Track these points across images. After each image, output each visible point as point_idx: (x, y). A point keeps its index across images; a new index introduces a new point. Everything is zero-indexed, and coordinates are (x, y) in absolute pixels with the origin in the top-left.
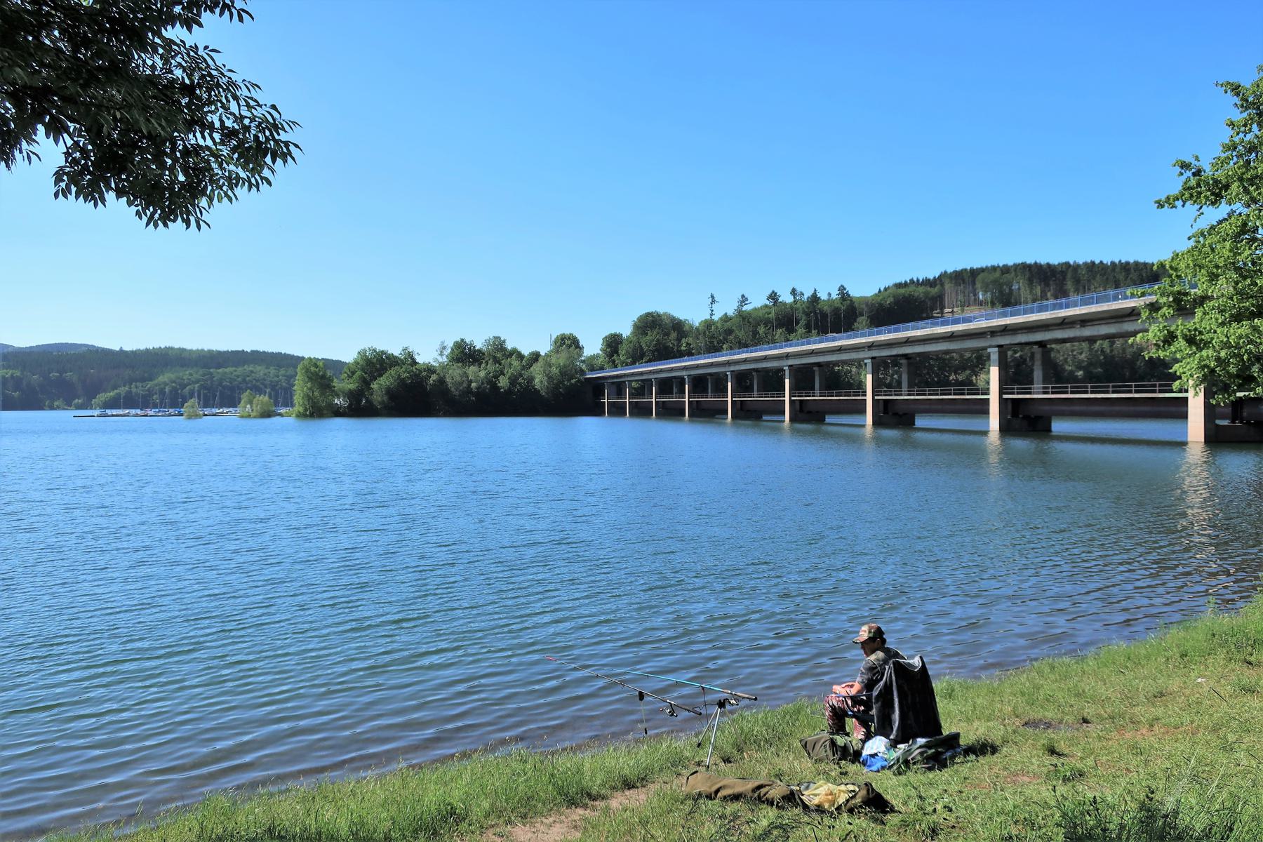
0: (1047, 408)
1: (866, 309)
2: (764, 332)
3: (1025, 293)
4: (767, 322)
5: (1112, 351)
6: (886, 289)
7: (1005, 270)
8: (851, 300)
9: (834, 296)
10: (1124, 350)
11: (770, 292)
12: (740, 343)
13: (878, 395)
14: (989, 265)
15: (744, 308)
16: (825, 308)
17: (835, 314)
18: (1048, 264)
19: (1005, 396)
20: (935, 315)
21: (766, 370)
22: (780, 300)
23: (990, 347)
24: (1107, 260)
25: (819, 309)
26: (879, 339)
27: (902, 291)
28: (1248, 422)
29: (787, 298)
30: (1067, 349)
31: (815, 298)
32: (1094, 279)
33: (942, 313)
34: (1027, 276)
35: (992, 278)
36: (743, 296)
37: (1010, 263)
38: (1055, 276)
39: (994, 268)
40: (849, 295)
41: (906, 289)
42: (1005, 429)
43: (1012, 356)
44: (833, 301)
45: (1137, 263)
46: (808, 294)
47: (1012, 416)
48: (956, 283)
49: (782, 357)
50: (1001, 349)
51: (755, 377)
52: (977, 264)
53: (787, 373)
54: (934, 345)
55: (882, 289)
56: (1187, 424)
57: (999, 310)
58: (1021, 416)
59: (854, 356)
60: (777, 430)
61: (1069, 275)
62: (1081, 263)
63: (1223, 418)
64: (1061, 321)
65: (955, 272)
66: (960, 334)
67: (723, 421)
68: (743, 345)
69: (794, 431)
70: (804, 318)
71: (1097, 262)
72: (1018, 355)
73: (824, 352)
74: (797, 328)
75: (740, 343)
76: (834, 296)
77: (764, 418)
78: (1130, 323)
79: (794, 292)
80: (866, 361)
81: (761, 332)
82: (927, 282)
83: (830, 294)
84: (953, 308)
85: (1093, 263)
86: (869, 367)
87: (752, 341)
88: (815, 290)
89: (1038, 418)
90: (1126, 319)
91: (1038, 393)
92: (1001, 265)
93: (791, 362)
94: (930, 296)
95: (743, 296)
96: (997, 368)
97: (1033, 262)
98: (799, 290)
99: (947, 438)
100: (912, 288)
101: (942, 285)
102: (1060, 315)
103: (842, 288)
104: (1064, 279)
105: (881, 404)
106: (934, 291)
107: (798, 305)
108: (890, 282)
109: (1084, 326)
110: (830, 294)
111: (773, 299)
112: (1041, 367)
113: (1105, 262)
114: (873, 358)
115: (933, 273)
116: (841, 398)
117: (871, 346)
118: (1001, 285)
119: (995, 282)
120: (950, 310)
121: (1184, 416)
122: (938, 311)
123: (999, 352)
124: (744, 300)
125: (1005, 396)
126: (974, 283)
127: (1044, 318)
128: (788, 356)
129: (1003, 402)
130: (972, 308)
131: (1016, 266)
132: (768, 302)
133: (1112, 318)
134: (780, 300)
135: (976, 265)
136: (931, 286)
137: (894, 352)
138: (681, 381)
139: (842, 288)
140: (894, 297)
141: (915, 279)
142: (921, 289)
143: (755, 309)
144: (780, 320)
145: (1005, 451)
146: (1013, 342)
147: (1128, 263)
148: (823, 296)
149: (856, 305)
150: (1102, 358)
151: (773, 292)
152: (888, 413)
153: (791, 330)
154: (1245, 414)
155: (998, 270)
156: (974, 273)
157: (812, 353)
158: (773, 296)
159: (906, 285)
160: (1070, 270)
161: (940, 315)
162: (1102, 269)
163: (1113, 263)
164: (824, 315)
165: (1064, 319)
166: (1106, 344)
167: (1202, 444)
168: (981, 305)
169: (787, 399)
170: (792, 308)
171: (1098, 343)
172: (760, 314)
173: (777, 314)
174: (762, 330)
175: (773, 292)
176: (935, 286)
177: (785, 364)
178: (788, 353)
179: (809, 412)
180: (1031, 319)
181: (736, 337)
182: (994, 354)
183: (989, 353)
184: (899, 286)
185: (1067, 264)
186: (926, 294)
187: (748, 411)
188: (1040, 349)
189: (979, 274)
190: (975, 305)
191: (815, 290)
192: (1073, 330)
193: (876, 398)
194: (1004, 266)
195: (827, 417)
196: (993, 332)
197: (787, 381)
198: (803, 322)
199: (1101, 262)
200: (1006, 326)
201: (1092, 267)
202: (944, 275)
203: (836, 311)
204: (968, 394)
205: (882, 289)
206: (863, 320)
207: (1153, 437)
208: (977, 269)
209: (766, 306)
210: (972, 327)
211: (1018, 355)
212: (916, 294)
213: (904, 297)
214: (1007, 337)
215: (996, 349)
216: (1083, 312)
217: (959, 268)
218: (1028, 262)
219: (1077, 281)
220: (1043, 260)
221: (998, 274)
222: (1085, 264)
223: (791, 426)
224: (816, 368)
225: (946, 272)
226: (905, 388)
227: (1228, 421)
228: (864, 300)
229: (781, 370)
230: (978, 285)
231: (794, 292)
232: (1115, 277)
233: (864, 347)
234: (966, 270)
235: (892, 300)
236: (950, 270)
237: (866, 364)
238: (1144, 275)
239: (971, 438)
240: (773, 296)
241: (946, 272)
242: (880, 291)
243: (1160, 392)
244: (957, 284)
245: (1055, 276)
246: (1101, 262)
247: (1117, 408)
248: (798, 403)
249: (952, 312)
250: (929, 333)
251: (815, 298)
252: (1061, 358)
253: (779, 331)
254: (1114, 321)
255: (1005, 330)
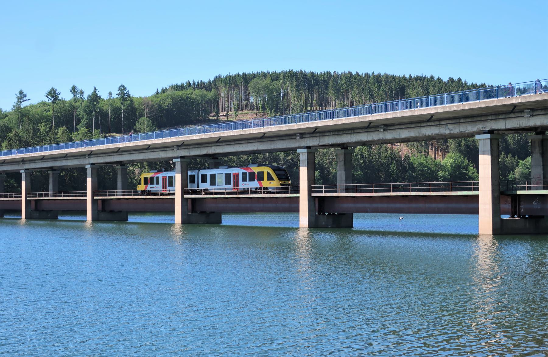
0: (351, 205)
1: (146, 110)
2: (45, 130)
3: (293, 99)
4: (48, 120)
5: (370, 155)
6: (164, 91)
7: (275, 77)
8: (131, 101)
9: (115, 96)
10: (380, 154)
11: (49, 89)
12: (20, 140)
13: (30, 197)
14: (260, 72)
15: (23, 105)
16: (105, 108)
17: (115, 113)
18: (312, 73)
19: (314, 195)
20: (211, 118)
21: (62, 169)
22: (60, 97)
23: (479, 133)
24: (362, 72)
25: (99, 108)
26: (190, 138)
27: (180, 93)
28: (524, 217)
29: (66, 96)
30: (332, 153)
31: (95, 98)
32: (352, 89)
33: (218, 116)
34: (294, 84)
35: (263, 84)
36: (21, 92)
37: (279, 71)
38: (317, 84)
39: (265, 75)
40: (129, 96)
41: (184, 91)
42: (314, 225)
43: (284, 159)
44: (114, 100)
45: (387, 76)
46: (88, 93)
47: (319, 214)
48: (230, 87)
49: (85, 155)
50: (310, 150)
51: (51, 176)
52: (249, 69)
53: (89, 172)
54: (244, 145)
55: (160, 91)
56: (478, 216)
57: (268, 117)
58: (326, 214)
59: (162, 155)
60: (78, 228)
61: (331, 83)
62: (340, 73)
63: (505, 213)
64: (367, 125)
65: (230, 77)
66: (272, 135)
67: (19, 221)
68: (25, 144)
69: (96, 231)
70: (86, 117)
71: (354, 73)
72: (289, 158)
73: (130, 151)
74: (78, 127)
75: (20, 140)
76: (115, 96)
77: (60, 218)
78: (428, 128)
79: (74, 90)
80: (174, 160)
81: (42, 130)
82: (201, 86)
83: (110, 94)
84: (227, 111)
85: (351, 74)
86: (178, 166)
87: (33, 139)
88: (95, 89)
89: (341, 215)
90: (425, 124)
91: (341, 192)
92: (270, 72)
93: (93, 160)
94: (206, 99)
95: (21, 92)
96: (306, 168)
97: (299, 70)
98: (79, 87)
99: (70, 223)
100: (189, 91)
101: (217, 88)
102: (367, 120)
103: (122, 88)
104: (326, 88)
105: (100, 203)
106: (210, 94)
107: (78, 104)
108: (167, 82)
109: (387, 130)
110: (110, 94)
111: (53, 97)
112: (343, 168)
113: (360, 74)
114: (182, 157)
115: (207, 77)
116: (148, 197)
117: (181, 145)
118: (271, 91)
119: (266, 87)
120: (225, 113)
121: (476, 211)
122: (213, 114)
123: (308, 153)
124: (22, 96)
125: (314, 195)
126: (246, 89)
127: (353, 121)
128: (91, 154)
129: (311, 199)
130: (245, 112)
131: (284, 73)
132: (46, 100)
133: (412, 123)
134: (60, 97)
135: (249, 71)
136: (206, 89)
137: (204, 151)
138: (17, 176)
139: (122, 88)
140: (172, 98)
141: (191, 82)
142: (198, 92)
143: (32, 106)
144: (60, 118)
145: (313, 245)
146: (321, 144)
147: (379, 75)
148: (104, 95)
149: (136, 105)
150: (362, 161)
151: (53, 89)
152: (196, 212)
153: (72, 129)
154: (522, 210)
155: (269, 77)
156: (246, 79)
157: (512, 112)
158: (53, 94)
159: (182, 87)
160: (332, 79)
161: (215, 118)
162: (359, 80)
163: (367, 74)
164: (104, 115)
165: (370, 123)
166: (365, 149)
167: (492, 235)
168: (253, 110)
169: (89, 198)
170: (71, 105)
171: (358, 148)
172: (39, 111)
173: (56, 112)
174: (43, 128)
175: (53, 89)
176: (211, 90)
177: (87, 163)
178: (92, 151)
179: (112, 212)
180: (340, 123)
181: (16, 134)
182: (303, 155)
183: (299, 154)
184: (176, 88)
185: (328, 74)
186: (203, 97)
187: (43, 211)
188: (343, 151)
189: (251, 80)
190: (246, 109)
191: (95, 89)
192: (377, 133)
193: (28, 199)
194: (273, 73)
195: (129, 217)
196: (303, 134)
197: (89, 180)
198: (84, 121)
199: (357, 73)
200: (316, 128)
201: (350, 78)
202: (218, 79)
203: (116, 110)
204: (393, 191)
205: (160, 91)
206: (144, 121)
207: (401, 229)
208: (249, 75)
209: (44, 103)
210: (284, 129)
211: (289, 158)
212: (193, 97)
213: (182, 99)
214: (315, 139)
215: (305, 150)
216: (389, 117)
217: (233, 73)
218: (295, 70)
219: (337, 90)
220: (307, 69)
221: (268, 80)
222: (344, 74)
223: (26, 221)
224: (118, 167)
225: (220, 76)
226: (341, 184)
227: (509, 216)
228: (144, 102)
229: (83, 170)
230: (251, 90)
231: (74, 90)
232: (369, 88)
233: (173, 147)
234: (239, 75)
235: (170, 101)
236: (224, 75)
237: (174, 163)
238: (393, 87)
239: (79, 224)
240: (53, 94)
241: (220, 76)
242: (157, 93)
243: (57, 197)
244: (231, 89)
245: (317, 84)
246: (357, 73)
247: (434, 205)
248: (33, 203)
249: (227, 115)
250: (242, 133)
251: (95, 98)
252: (327, 161)
253: (61, 129)
254: (413, 126)
255: (315, 132)
